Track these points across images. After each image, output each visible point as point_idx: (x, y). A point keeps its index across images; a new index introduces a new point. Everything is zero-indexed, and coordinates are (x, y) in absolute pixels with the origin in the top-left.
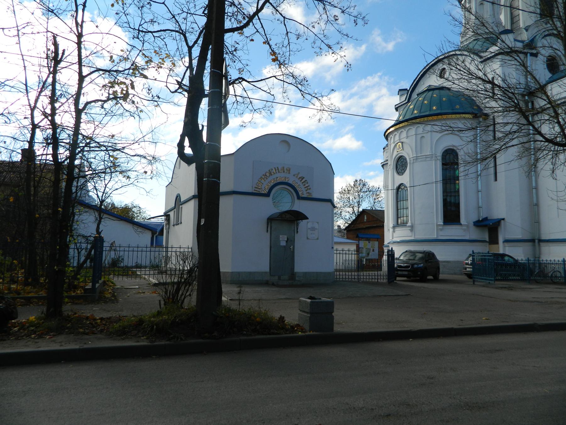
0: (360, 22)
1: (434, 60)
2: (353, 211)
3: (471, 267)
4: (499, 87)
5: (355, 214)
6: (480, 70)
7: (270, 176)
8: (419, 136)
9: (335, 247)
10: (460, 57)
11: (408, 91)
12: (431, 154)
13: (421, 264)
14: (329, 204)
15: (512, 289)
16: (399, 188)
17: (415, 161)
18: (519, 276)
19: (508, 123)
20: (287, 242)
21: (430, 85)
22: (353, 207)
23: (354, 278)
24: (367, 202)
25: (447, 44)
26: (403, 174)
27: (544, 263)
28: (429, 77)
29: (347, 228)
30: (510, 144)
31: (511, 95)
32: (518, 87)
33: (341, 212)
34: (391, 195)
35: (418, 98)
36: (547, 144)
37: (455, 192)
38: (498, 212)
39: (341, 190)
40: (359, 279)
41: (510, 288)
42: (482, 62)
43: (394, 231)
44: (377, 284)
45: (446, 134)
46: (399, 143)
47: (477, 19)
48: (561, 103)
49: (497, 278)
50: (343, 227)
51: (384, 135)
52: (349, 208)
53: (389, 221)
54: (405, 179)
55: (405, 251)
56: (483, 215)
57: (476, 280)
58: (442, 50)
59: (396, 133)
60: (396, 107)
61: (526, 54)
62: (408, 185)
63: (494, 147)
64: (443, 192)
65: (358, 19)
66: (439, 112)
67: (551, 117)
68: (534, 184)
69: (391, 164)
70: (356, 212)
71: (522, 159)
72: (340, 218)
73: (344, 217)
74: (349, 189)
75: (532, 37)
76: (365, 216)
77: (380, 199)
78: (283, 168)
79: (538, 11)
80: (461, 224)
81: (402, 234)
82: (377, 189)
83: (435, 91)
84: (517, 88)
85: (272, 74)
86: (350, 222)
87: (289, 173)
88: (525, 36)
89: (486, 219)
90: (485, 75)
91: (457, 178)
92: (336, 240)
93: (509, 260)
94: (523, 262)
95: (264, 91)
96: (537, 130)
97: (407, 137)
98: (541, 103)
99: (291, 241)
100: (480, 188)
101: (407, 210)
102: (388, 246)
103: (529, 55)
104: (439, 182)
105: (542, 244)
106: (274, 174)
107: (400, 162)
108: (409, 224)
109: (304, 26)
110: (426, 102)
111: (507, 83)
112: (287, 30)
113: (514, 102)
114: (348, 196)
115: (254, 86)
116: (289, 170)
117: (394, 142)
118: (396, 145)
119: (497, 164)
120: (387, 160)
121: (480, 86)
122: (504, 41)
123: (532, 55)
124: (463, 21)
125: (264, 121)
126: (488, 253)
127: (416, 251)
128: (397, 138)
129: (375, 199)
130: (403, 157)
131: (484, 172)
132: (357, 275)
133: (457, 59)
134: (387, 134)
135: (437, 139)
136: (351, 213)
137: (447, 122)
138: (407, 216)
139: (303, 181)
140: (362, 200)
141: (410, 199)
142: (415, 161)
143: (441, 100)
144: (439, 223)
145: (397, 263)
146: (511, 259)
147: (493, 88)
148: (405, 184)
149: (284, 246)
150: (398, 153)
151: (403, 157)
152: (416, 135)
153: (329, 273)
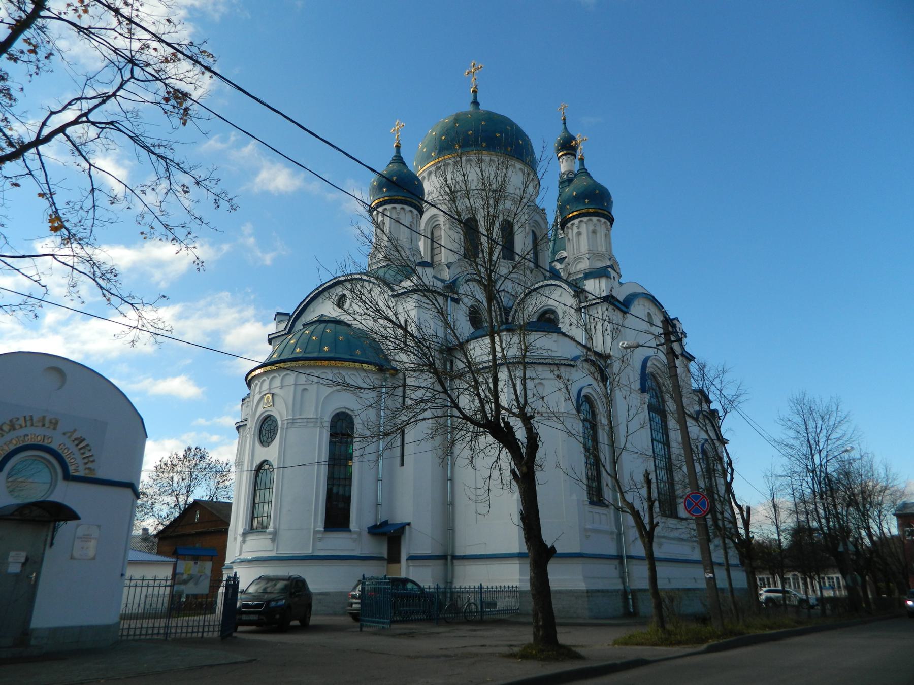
0: (224, 204)
1: (331, 280)
2: (176, 503)
3: (359, 601)
4: (412, 336)
5: (180, 509)
6: (389, 307)
7: (10, 430)
8: (300, 388)
9: (130, 572)
10: (366, 284)
11: (291, 317)
12: (315, 417)
13: (282, 599)
14: (128, 492)
15: (413, 637)
16: (260, 468)
17: (290, 425)
18: (424, 613)
19: (419, 387)
20: (24, 564)
21: (322, 315)
22: (177, 496)
23: (158, 633)
24: (205, 488)
25: (352, 265)
26: (269, 444)
27: (458, 592)
28: (323, 303)
29: (160, 534)
30: (421, 417)
31: (425, 350)
32: (434, 340)
33: (153, 504)
34: (246, 480)
35: (303, 331)
36: (464, 421)
37: (345, 479)
38: (403, 513)
39: (160, 463)
40: (167, 634)
41: (411, 635)
42: (393, 296)
43: (244, 541)
44: (202, 642)
45: (337, 390)
46: (269, 395)
47: (391, 241)
48: (484, 368)
49: (395, 619)
50: (152, 531)
51: (246, 379)
52: (169, 496)
53: (238, 522)
54: (271, 453)
55: (258, 577)
56: (382, 517)
57: (365, 623)
58: (344, 269)
59: (265, 378)
60: (270, 337)
61: (446, 297)
62: (275, 466)
63: (400, 418)
64: (328, 478)
65: (221, 201)
66: (332, 355)
67: (471, 386)
68: (449, 475)
69: (252, 426)
70: (182, 503)
71: (435, 439)
72: (151, 514)
73: (157, 512)
74: (174, 462)
75: (455, 278)
76: (198, 512)
77: (227, 483)
78: (44, 418)
79: (462, 251)
80: (350, 531)
81: (257, 546)
82: (225, 465)
83: (329, 325)
84: (433, 342)
85: (51, 249)
86: (167, 523)
87: (54, 429)
88: (446, 275)
89: (385, 523)
90: (396, 315)
91: (351, 458)
92: (133, 555)
93: (412, 589)
94: (431, 590)
95: (26, 276)
96: (454, 401)
97: (282, 387)
98: (460, 365)
99: (33, 563)
100: (380, 476)
101: (270, 505)
102: (231, 568)
103: (449, 299)
104: (323, 463)
105: (455, 562)
106: (21, 427)
107: (266, 425)
108: (271, 529)
109: (126, 186)
110: (314, 338)
111: (422, 333)
112: (92, 185)
113: (428, 359)
114: (171, 475)
115: (6, 263)
116: (55, 424)
117: (260, 392)
118: (262, 398)
119: (405, 443)
120: (246, 420)
121: (388, 329)
122: (421, 277)
123: (453, 300)
124: (374, 241)
125: (19, 329)
126: (385, 578)
127: (277, 576)
128: (266, 386)
129: (218, 483)
130: (272, 418)
131: (387, 453)
132: (165, 627)
133: (363, 287)
134: (250, 377)
135: (326, 395)
136: (173, 505)
137: (341, 372)
138: (269, 516)
139: (80, 446)
140: (195, 484)
141: (276, 486)
142: (290, 425)
143: (336, 339)
144: (317, 529)
145: (241, 599)
146: (415, 587)
147: (405, 336)
148: (270, 462)
149: (16, 575)
150: (265, 409)
151: (272, 418)
152: (295, 384)
153: (107, 628)
